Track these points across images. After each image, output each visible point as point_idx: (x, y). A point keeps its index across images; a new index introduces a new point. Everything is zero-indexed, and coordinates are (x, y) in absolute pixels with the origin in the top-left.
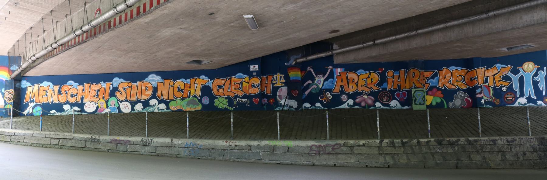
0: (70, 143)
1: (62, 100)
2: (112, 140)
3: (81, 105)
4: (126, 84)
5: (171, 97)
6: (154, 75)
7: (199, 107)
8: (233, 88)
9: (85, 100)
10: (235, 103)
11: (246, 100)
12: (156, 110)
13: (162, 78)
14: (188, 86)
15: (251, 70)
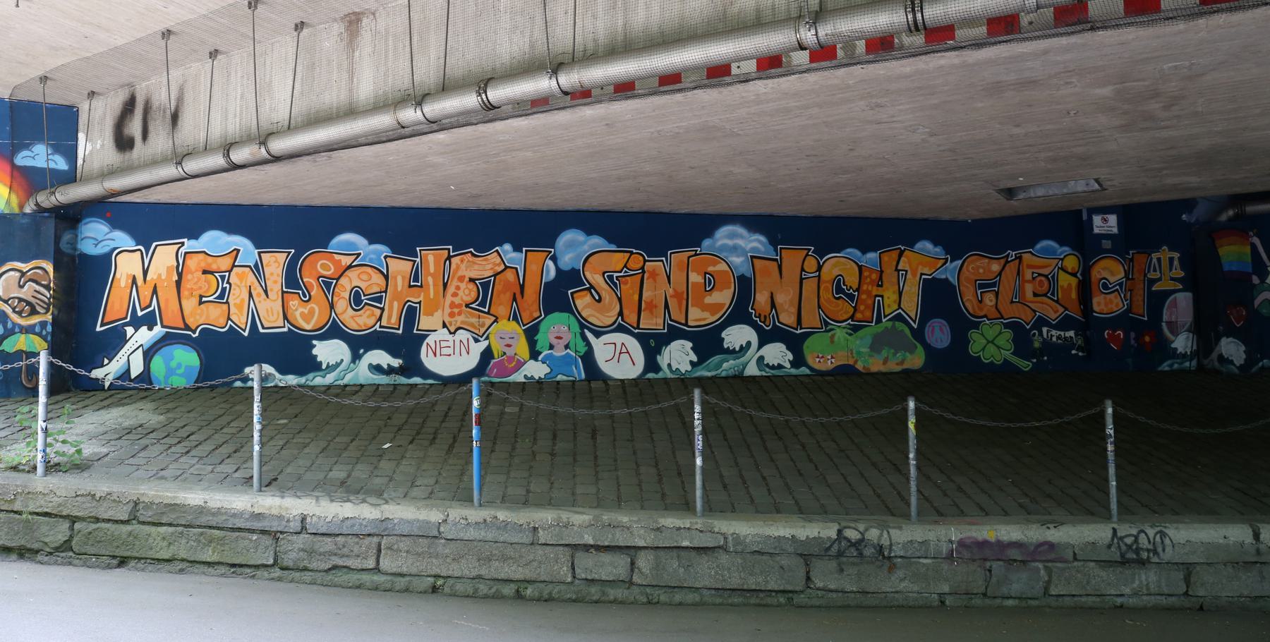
0: (705, 573)
1: (307, 318)
2: (961, 543)
3: (406, 344)
4: (618, 260)
5: (811, 318)
6: (740, 230)
7: (916, 360)
8: (1029, 289)
9: (424, 322)
10: (1037, 345)
11: (1071, 333)
12: (752, 370)
13: (774, 242)
14: (874, 276)
15: (1096, 231)
